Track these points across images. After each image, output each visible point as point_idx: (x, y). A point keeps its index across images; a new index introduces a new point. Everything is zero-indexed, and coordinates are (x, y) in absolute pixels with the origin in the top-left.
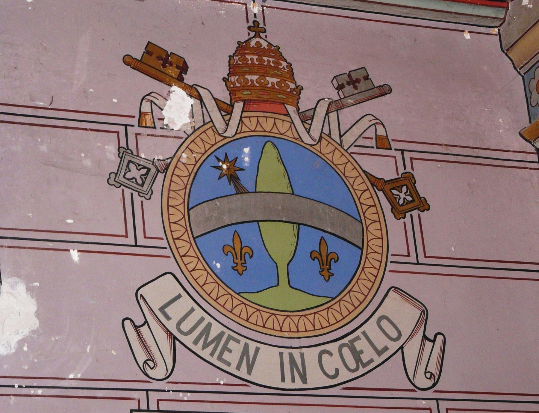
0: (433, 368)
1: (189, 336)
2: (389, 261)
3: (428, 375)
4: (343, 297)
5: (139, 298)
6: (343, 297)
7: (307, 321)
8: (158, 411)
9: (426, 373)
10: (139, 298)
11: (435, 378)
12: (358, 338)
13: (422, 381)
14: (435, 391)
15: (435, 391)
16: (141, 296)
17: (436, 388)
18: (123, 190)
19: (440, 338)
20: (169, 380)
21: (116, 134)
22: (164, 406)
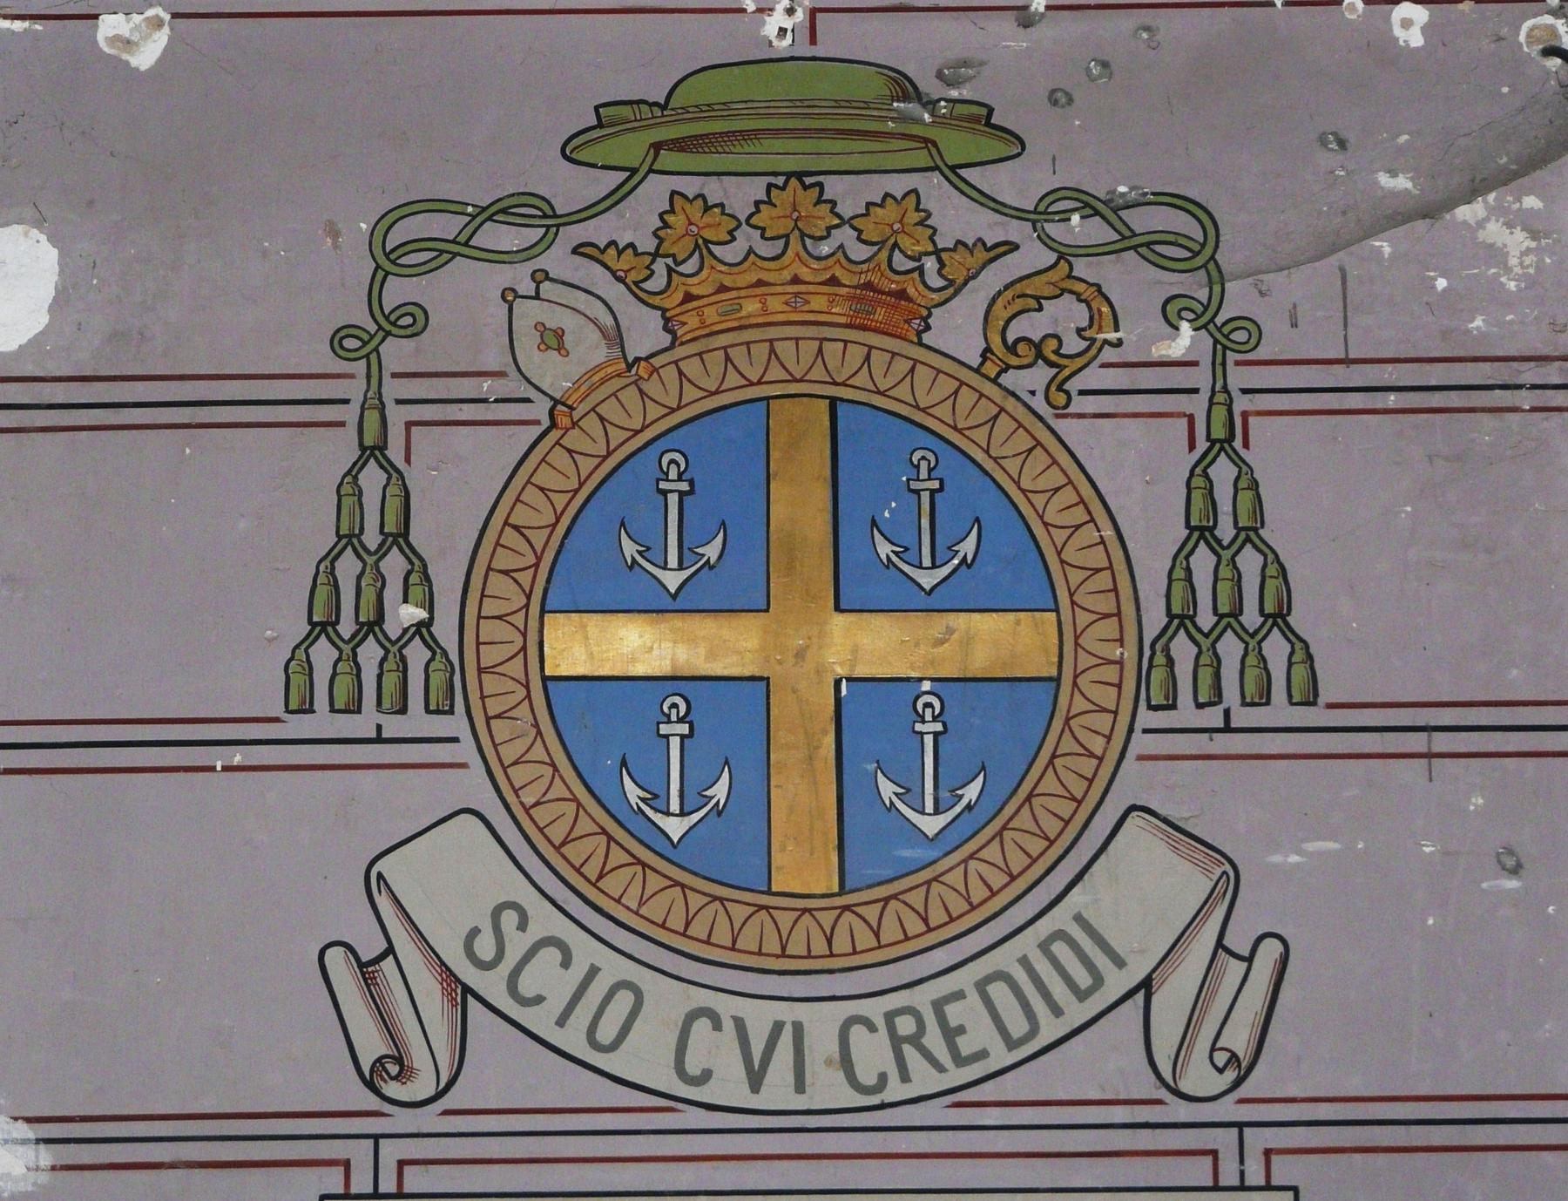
0: (1239, 1039)
1: (503, 986)
2: (1138, 726)
3: (1221, 1058)
4: (1011, 819)
5: (373, 883)
6: (1011, 819)
7: (858, 925)
8: (400, 1194)
9: (1213, 1049)
10: (373, 883)
11: (1242, 1068)
12: (959, 995)
13: (1200, 1077)
14: (1241, 1101)
15: (1241, 1101)
16: (380, 876)
17: (1245, 1091)
18: (538, 423)
19: (1271, 949)
20: (446, 1102)
21: (819, 15)
22: (416, 1181)
